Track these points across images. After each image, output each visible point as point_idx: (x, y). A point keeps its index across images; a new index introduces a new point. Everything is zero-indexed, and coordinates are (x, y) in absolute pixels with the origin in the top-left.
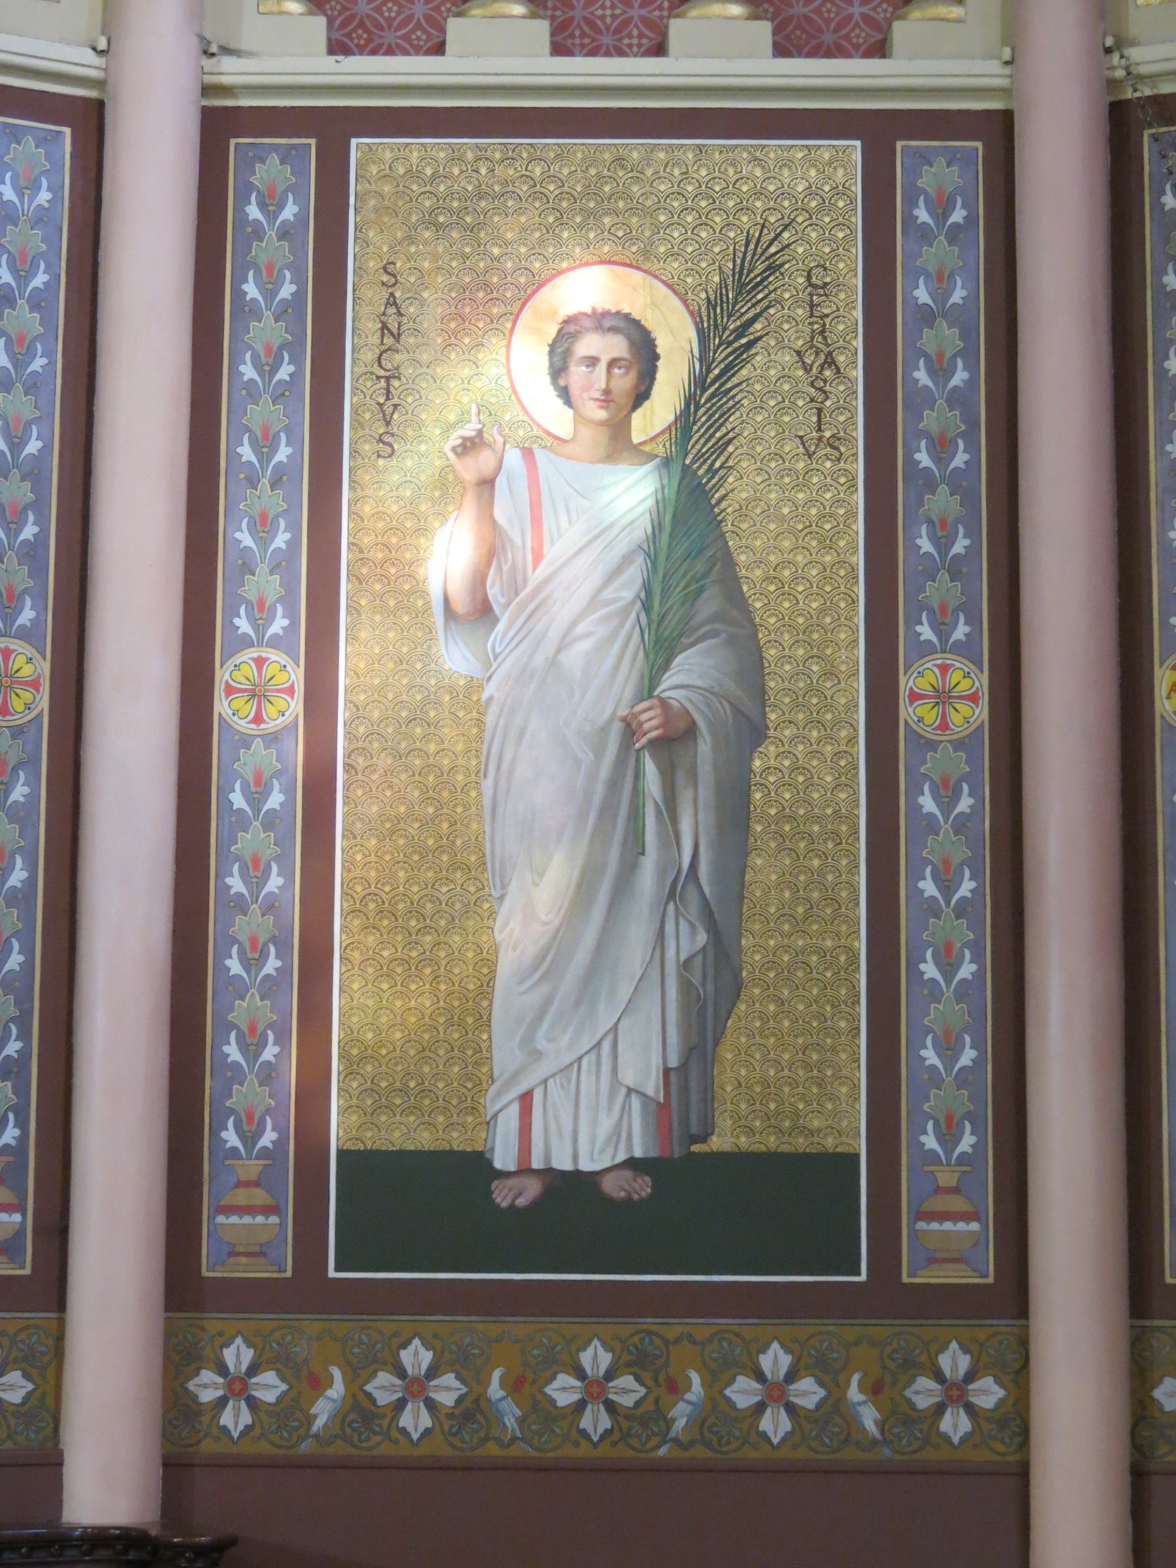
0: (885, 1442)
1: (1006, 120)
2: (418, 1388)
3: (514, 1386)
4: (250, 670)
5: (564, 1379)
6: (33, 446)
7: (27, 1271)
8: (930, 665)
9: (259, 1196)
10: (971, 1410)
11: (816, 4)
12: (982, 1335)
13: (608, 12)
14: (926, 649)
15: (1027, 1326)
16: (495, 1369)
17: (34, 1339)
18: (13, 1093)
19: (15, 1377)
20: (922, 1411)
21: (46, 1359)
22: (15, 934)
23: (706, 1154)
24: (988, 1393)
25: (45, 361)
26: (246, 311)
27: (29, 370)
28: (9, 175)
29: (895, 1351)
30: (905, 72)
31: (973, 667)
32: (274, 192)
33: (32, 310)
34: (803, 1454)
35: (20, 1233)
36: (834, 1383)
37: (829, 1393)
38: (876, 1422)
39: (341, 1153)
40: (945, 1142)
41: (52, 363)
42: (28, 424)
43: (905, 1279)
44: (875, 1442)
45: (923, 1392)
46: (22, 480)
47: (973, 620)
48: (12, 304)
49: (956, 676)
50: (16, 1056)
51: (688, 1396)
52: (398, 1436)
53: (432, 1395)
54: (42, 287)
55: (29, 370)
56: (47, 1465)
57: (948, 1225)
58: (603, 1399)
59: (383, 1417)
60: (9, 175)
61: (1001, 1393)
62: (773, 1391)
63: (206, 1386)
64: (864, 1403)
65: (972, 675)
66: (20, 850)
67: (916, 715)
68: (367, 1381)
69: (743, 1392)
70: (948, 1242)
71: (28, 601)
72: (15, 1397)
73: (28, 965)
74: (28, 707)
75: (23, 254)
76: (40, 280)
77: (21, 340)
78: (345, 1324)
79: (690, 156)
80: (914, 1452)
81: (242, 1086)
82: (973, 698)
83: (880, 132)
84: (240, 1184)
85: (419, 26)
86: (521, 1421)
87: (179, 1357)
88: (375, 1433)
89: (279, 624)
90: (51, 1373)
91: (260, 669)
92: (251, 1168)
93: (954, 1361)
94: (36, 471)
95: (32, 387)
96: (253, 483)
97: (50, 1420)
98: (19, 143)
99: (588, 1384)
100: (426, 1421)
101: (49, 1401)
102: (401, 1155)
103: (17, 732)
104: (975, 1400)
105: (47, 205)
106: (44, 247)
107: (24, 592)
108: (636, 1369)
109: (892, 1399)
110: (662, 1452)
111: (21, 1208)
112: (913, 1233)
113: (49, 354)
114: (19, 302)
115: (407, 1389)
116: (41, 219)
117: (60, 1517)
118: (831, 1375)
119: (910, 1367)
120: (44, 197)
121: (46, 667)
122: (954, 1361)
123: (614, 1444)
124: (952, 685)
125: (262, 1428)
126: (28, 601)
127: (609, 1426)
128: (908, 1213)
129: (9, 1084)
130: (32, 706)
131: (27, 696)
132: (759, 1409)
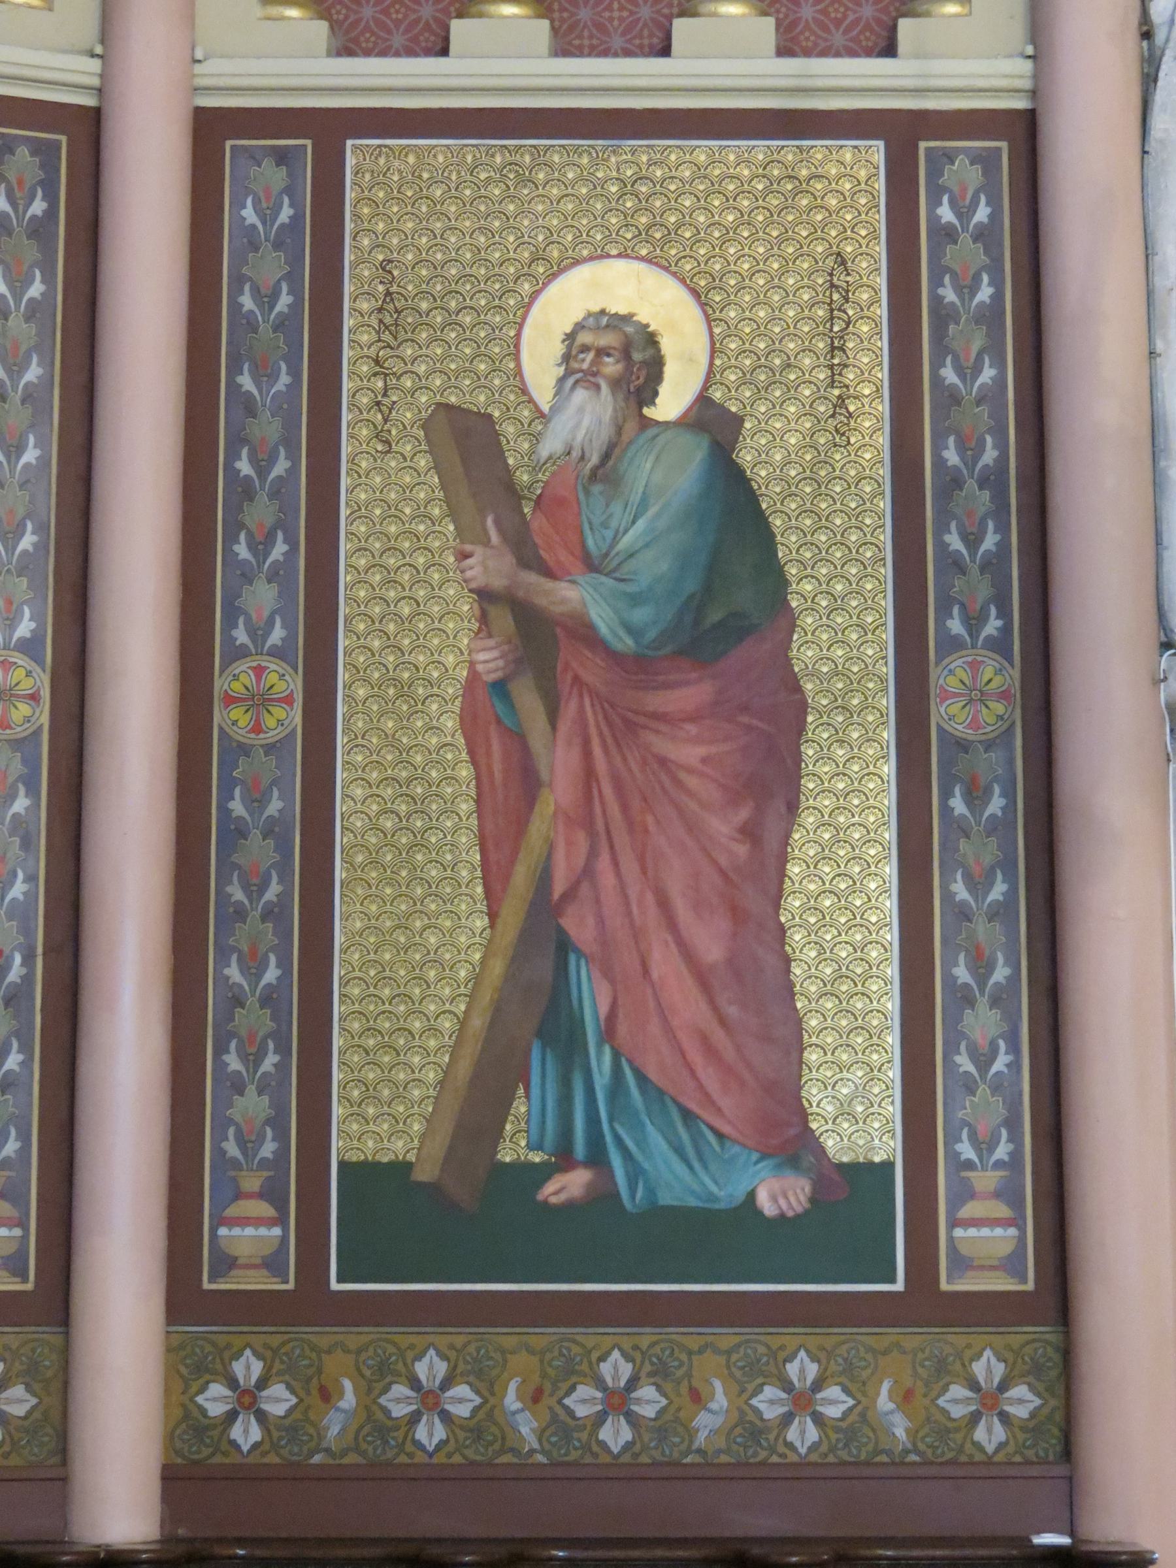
3: (905, 1398)
4: (248, 679)
7: (290, 1286)
8: (242, 667)
11: (606, 3)
12: (829, 1342)
13: (616, 14)
14: (241, 653)
19: (18, 1391)
21: (49, 1374)
22: (272, 949)
31: (289, 668)
32: (262, 201)
36: (489, 1387)
37: (301, 1400)
38: (907, 1430)
39: (342, 1165)
43: (944, 1286)
45: (583, 1401)
53: (819, 1408)
59: (397, 1429)
63: (1023, 1401)
64: (522, 1410)
67: (232, 720)
72: (19, 1410)
79: (527, 159)
83: (905, 135)
85: (367, 28)
86: (540, 1434)
87: (186, 1367)
89: (277, 635)
100: (440, 1433)
102: (364, 1164)
103: (17, 744)
104: (265, 1407)
109: (550, 1408)
111: (282, 1220)
112: (951, 1240)
115: (255, 1399)
118: (858, 1385)
119: (943, 1371)
124: (13, 684)
127: (444, 1437)
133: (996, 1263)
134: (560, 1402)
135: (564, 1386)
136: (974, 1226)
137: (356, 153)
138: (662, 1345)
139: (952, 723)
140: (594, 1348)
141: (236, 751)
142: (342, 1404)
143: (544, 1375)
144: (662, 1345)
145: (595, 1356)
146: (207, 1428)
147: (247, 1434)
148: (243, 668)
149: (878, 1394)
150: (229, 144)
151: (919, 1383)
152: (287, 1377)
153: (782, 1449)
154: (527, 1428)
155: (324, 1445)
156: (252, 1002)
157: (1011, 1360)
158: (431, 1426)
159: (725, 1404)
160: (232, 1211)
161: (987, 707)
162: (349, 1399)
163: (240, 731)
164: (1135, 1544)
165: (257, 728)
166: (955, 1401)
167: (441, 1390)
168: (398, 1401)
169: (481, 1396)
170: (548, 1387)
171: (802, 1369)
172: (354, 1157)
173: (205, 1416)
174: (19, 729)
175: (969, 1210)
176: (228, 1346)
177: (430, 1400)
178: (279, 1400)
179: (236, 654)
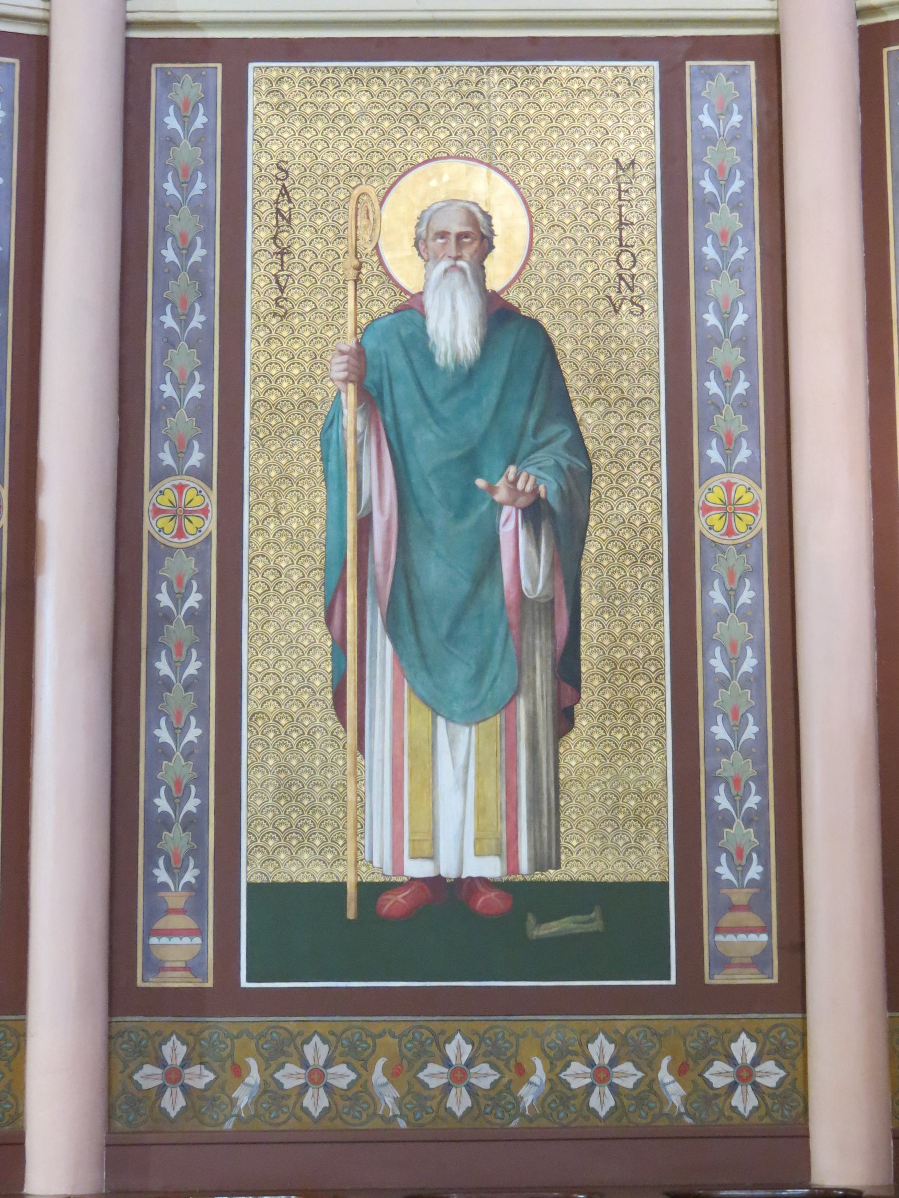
0: (543, 1115)
1: (775, 41)
3: (393, 1073)
5: (719, 1066)
6: (740, 319)
7: (775, 980)
8: (717, 481)
14: (716, 470)
16: (664, 1057)
17: (784, 1035)
18: (756, 837)
20: (717, 1089)
21: (795, 1050)
23: (560, 883)
24: (770, 1074)
25: (745, 249)
26: (167, 208)
27: (733, 259)
28: (706, 106)
32: (183, 107)
33: (732, 211)
35: (768, 948)
36: (649, 1066)
39: (249, 885)
40: (738, 868)
41: (751, 250)
42: (735, 302)
44: (681, 1114)
46: (733, 347)
48: (715, 207)
49: (189, 494)
50: (756, 808)
51: (534, 1079)
52: (302, 1114)
54: (739, 191)
55: (733, 259)
57: (742, 937)
60: (706, 106)
64: (673, 1082)
66: (750, 642)
67: (155, 527)
69: (290, 1076)
70: (740, 947)
71: (744, 443)
73: (762, 734)
74: (749, 527)
75: (721, 168)
76: (737, 185)
77: (724, 235)
78: (625, 1022)
81: (731, 828)
86: (399, 1102)
89: (196, 458)
90: (799, 1062)
91: (181, 494)
93: (744, 1048)
94: (744, 338)
95: (736, 271)
97: (800, 1100)
98: (713, 80)
99: (457, 1072)
101: (799, 1085)
102: (313, 885)
105: (738, 126)
106: (739, 159)
107: (740, 436)
108: (492, 1058)
110: (514, 1124)
111: (766, 929)
112: (146, 946)
113: (749, 244)
114: (721, 206)
116: (734, 137)
117: (810, 1179)
118: (360, 1061)
120: (736, 118)
121: (762, 494)
122: (316, 1050)
123: (332, 1120)
126: (744, 443)
128: (709, 925)
129: (751, 830)
130: (753, 527)
131: (748, 518)
132: (446, 1089)
135: (418, 1065)
137: (256, 71)
141: (161, 552)
142: (248, 1080)
143: (403, 1056)
144: (638, 1030)
145: (299, 1041)
147: (745, 1101)
149: (659, 1069)
150: (17, 61)
151: (405, 1062)
154: (389, 1097)
157: (192, 1045)
160: (160, 924)
162: (539, 1076)
163: (165, 536)
165: (180, 533)
167: (308, 1068)
170: (691, 1063)
172: (257, 879)
173: (712, 1088)
174: (192, 538)
175: (729, 919)
177: (744, 1075)
179: (161, 474)
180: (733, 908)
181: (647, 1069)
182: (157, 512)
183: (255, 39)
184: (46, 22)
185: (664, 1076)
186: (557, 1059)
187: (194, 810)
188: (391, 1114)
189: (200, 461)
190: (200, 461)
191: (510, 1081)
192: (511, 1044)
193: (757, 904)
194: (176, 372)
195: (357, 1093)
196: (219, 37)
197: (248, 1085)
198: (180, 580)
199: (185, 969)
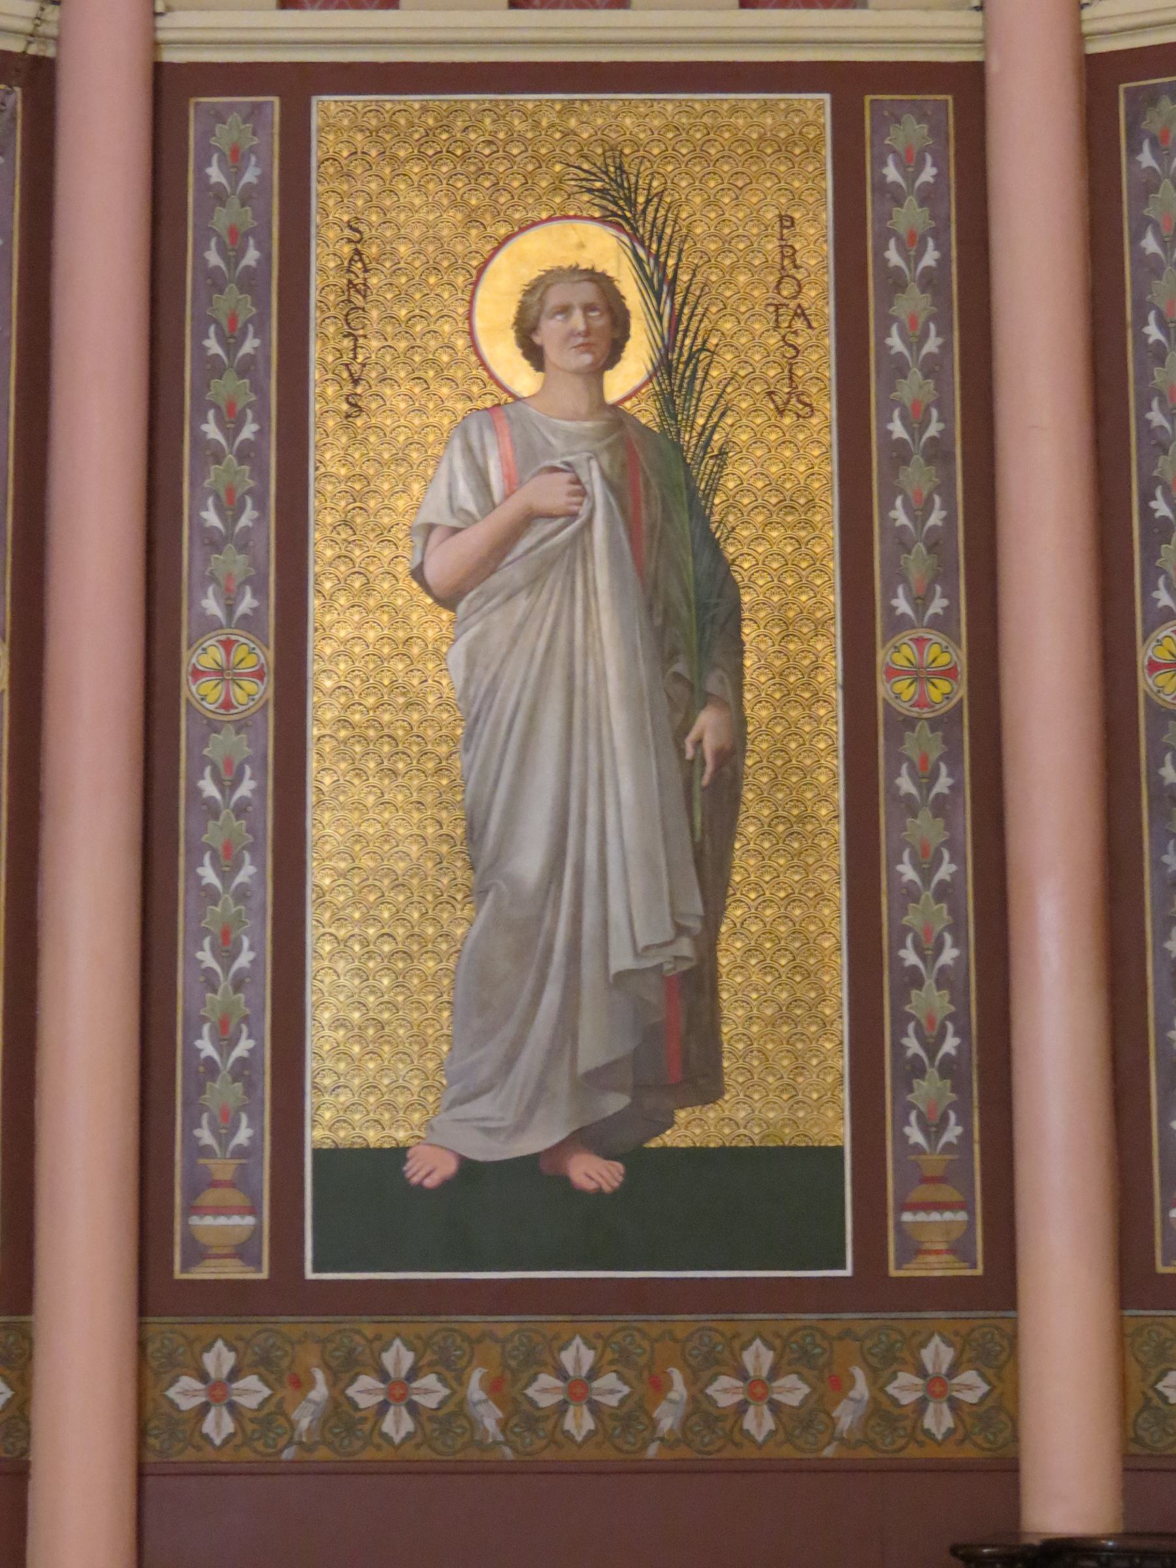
2: (402, 1391)
3: (494, 1388)
7: (264, 1275)
9: (954, 1196)
10: (414, 1409)
12: (606, 1329)
15: (1016, 1319)
20: (724, 1408)
24: (971, 1386)
29: (875, 1346)
30: (409, 24)
32: (230, 152)
34: (425, 1453)
38: (498, 1421)
39: (317, 1152)
41: (266, 344)
43: (893, 1272)
45: (544, 1391)
47: (260, 592)
49: (239, 653)
56: (1004, 1472)
58: (928, 1396)
61: (172, 1393)
62: (758, 1390)
64: (485, 1401)
65: (950, 650)
67: (896, 692)
68: (528, 1384)
69: (724, 1391)
70: (934, 1237)
80: (719, 1451)
82: (197, 674)
83: (850, 85)
84: (926, 1180)
86: (503, 1425)
88: (1168, 1434)
91: (228, 653)
92: (935, 1161)
95: (246, 368)
96: (218, 458)
99: (578, 1384)
111: (254, 1210)
114: (929, 1070)
123: (237, 1447)
125: (965, 1427)
131: (944, 686)
133: (225, 1251)
134: (1153, 1387)
136: (223, 1214)
138: (986, 1330)
139: (204, 703)
140: (734, 1337)
142: (672, 1395)
146: (717, 1419)
148: (1168, 632)
152: (438, 1369)
153: (377, 1439)
154: (489, 1417)
155: (659, 1434)
156: (224, 984)
158: (759, 1416)
159: (685, 1393)
161: (240, 687)
164: (1045, 1534)
166: (544, 1390)
168: (365, 1391)
169: (989, 1383)
171: (398, 1358)
175: (210, 1197)
176: (556, 1337)
178: (611, 1389)
179: (897, 624)
180: (215, 1184)
181: (454, 1384)
182: (197, 674)
183: (612, 63)
184: (57, 40)
185: (475, 1390)
186: (343, 1370)
187: (953, 1052)
188: (490, 1440)
189: (943, 608)
190: (943, 608)
191: (283, 1399)
192: (645, 1352)
193: (243, 1181)
194: (910, 493)
195: (270, 1414)
196: (532, 60)
197: (310, 1401)
198: (228, 763)
199: (948, 1251)
